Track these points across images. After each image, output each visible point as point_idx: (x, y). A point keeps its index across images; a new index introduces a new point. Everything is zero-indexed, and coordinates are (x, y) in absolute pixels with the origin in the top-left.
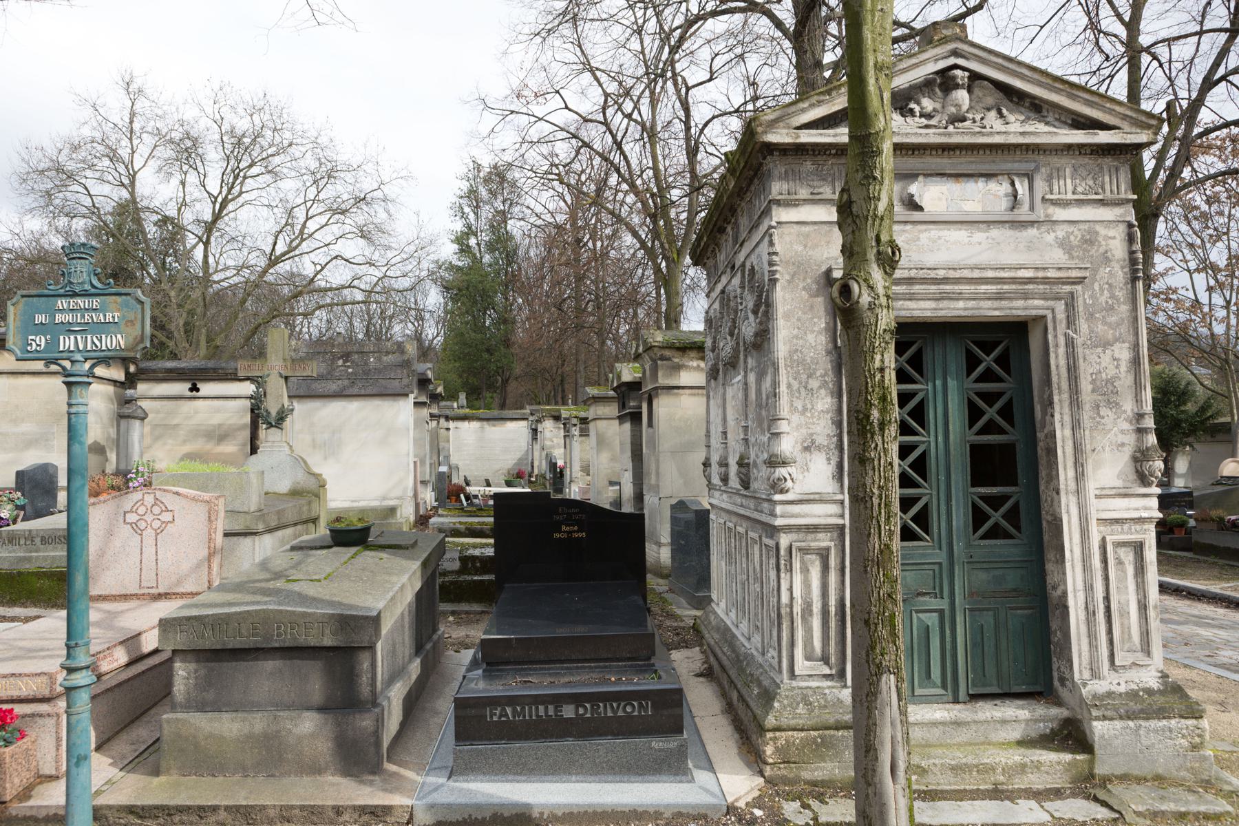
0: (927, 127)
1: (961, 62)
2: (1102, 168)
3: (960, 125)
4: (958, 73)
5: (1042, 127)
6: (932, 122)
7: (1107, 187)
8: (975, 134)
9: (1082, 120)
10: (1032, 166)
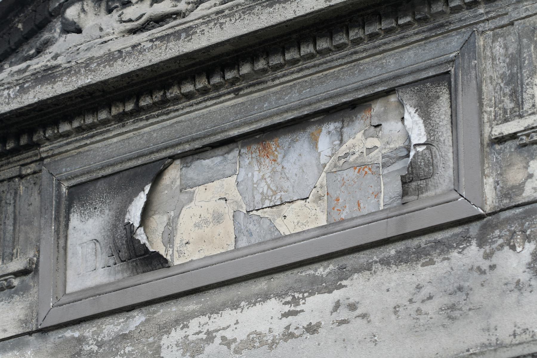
10: (452, 44)
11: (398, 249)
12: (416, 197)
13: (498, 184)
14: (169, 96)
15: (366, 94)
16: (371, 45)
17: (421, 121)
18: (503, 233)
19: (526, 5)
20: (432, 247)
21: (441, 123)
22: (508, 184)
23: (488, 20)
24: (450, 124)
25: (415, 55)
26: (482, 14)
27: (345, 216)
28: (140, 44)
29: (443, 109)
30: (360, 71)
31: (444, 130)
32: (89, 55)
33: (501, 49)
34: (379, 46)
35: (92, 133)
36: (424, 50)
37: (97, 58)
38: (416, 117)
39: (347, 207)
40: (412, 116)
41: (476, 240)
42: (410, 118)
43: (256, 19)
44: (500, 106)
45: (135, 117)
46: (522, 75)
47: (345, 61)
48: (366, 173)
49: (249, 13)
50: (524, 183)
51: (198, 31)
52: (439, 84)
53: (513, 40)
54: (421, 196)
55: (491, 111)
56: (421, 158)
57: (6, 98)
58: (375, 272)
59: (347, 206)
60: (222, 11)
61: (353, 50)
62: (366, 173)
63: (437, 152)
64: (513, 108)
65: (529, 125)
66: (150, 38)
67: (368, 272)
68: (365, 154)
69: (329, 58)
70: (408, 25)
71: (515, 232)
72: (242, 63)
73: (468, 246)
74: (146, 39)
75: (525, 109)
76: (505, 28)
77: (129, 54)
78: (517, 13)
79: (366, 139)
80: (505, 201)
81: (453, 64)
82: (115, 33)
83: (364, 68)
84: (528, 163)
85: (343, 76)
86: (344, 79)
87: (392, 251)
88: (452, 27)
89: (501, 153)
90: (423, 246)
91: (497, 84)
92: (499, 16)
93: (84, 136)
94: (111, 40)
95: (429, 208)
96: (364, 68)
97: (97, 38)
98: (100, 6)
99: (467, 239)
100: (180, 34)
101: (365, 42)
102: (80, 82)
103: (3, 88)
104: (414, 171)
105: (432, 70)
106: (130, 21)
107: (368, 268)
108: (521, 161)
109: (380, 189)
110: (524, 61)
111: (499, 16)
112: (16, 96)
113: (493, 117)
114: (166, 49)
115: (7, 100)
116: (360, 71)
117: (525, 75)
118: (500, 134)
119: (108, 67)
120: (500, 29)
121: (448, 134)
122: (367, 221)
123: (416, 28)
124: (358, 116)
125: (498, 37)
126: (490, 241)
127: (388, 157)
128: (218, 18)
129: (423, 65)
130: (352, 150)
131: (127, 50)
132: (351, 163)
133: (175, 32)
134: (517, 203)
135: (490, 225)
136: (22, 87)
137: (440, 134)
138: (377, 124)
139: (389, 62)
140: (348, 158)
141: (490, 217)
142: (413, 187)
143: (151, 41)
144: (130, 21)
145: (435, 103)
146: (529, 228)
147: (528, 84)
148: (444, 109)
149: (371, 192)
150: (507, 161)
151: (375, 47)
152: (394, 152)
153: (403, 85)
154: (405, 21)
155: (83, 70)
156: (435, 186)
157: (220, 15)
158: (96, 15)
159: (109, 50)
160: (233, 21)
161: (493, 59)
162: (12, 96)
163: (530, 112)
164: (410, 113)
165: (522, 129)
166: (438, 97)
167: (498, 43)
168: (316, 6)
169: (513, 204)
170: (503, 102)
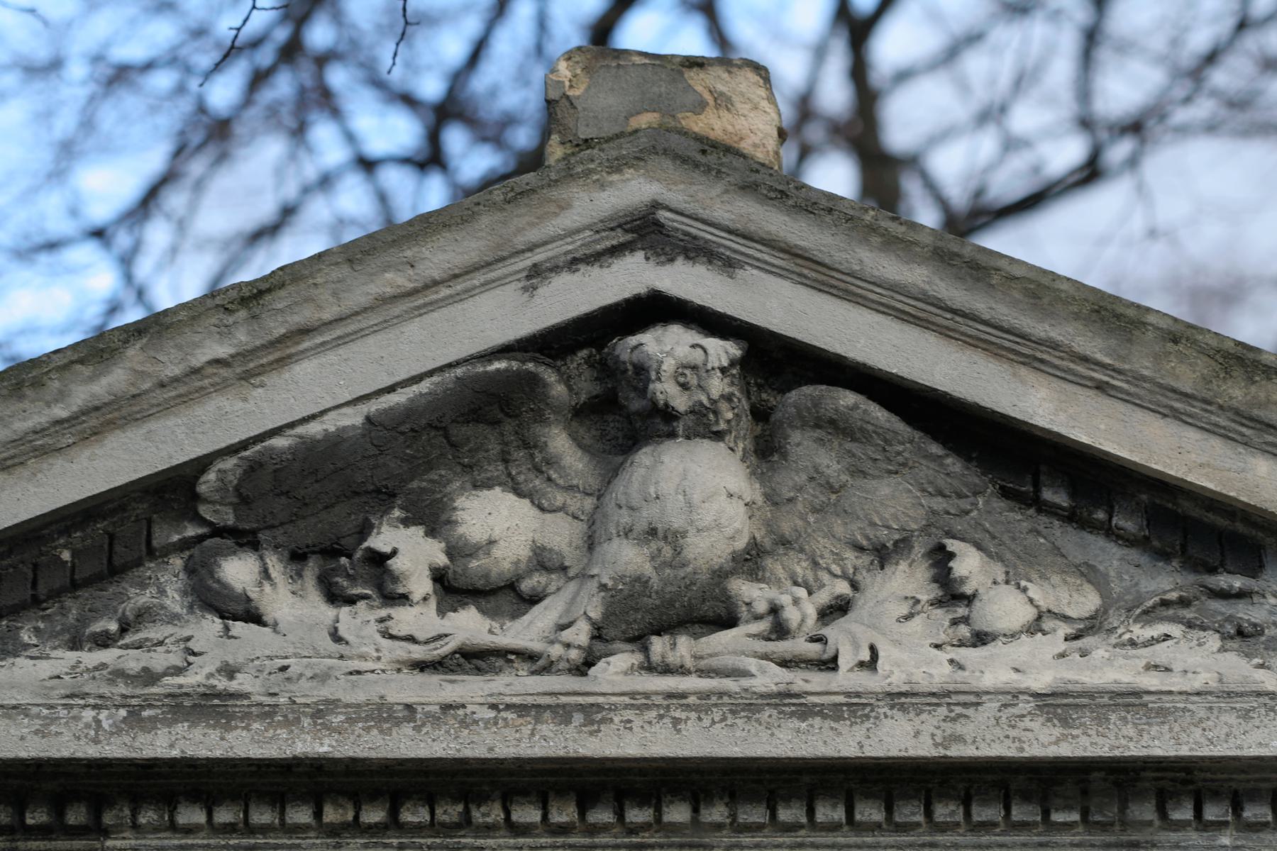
0: (474, 659)
1: (685, 281)
3: (684, 648)
4: (667, 346)
5: (1197, 660)
6: (526, 631)
8: (750, 706)
14: (477, 815)
28: (464, 706)
32: (325, 692)
35: (253, 841)
37: (347, 706)
43: (765, 735)
45: (372, 837)
49: (749, 718)
51: (616, 719)
57: (88, 726)
60: (683, 695)
61: (928, 839)
66: (490, 700)
69: (869, 840)
72: (669, 797)
74: (482, 700)
77: (435, 720)
82: (383, 660)
93: (231, 842)
94: (373, 671)
97: (330, 657)
98: (300, 575)
100: (570, 712)
101: (961, 831)
102: (300, 745)
103: (82, 702)
106: (411, 639)
112: (119, 732)
114: (533, 734)
115: (92, 733)
119: (375, 732)
121: (159, 750)
123: (1079, 834)
128: (668, 707)
131: (427, 708)
133: (558, 705)
136: (134, 714)
143: (494, 707)
144: (411, 639)
155: (306, 722)
157: (675, 701)
158: (293, 593)
159: (382, 697)
160: (706, 722)
162: (105, 725)
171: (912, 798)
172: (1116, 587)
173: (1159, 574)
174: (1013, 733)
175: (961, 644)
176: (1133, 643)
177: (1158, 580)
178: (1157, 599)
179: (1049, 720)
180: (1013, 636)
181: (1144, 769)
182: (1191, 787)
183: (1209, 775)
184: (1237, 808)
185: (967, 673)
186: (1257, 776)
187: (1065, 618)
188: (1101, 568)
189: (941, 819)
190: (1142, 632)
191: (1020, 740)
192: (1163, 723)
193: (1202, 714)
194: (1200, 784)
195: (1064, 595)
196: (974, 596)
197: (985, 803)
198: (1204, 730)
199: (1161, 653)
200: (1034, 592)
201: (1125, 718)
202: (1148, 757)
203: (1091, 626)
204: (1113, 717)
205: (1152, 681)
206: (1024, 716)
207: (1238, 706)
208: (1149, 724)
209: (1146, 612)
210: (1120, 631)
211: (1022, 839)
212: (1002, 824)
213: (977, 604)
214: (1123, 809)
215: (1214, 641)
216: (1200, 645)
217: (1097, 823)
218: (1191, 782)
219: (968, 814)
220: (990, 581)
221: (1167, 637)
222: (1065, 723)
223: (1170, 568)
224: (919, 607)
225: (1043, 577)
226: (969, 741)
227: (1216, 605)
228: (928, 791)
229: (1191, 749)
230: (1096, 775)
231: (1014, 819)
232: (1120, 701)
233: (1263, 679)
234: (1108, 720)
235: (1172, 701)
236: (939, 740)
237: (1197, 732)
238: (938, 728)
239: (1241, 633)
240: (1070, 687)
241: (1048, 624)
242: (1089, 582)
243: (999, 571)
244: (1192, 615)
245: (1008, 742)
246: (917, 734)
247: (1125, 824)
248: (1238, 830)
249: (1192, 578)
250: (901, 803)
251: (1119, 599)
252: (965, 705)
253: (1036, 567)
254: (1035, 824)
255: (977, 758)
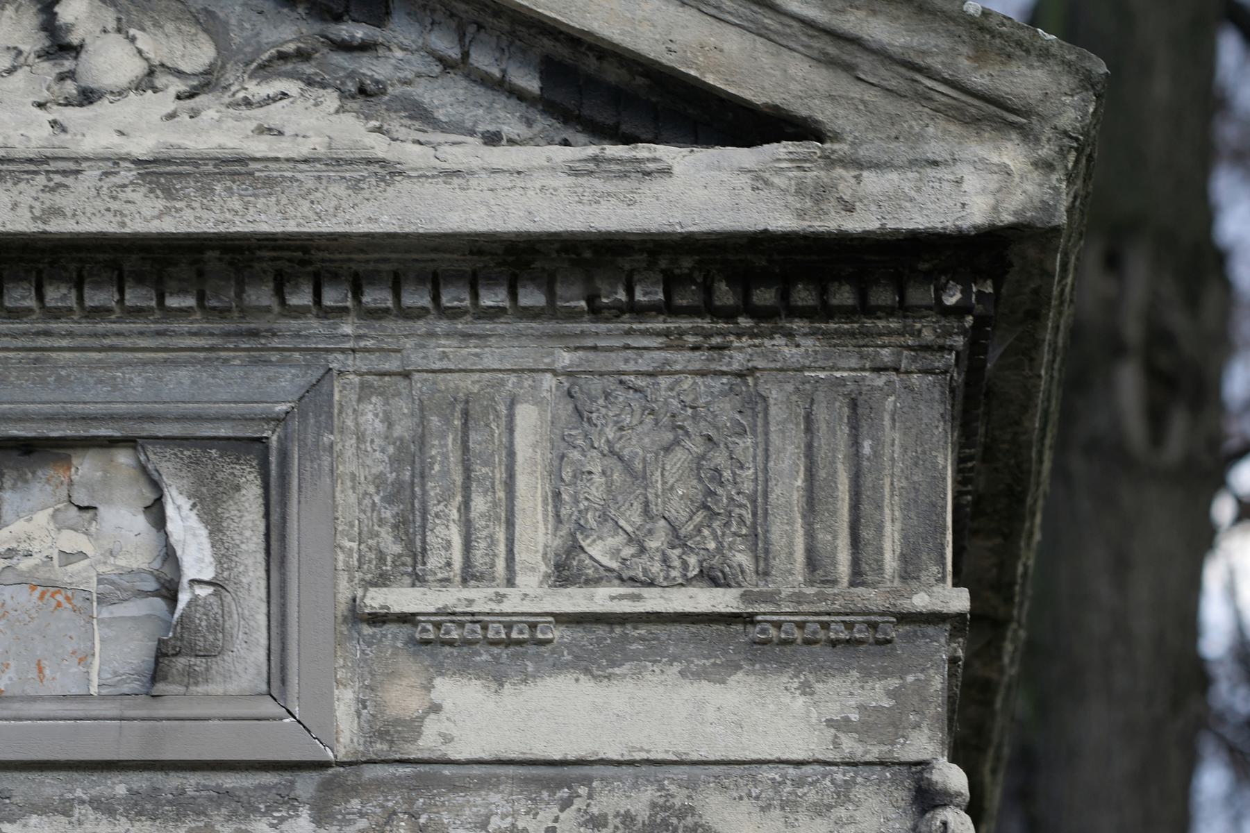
2: (755, 404)
5: (311, 121)
7: (788, 535)
9: (613, 74)
10: (281, 387)
11: (135, 787)
12: (182, 689)
13: (365, 707)
15: (69, 433)
16: (86, 326)
17: (203, 532)
18: (369, 808)
19: (444, 346)
20: (210, 799)
21: (243, 546)
22: (388, 712)
23: (354, 351)
24: (263, 552)
25: (193, 382)
26: (347, 336)
27: (6, 685)
29: (248, 517)
30: (59, 379)
31: (250, 562)
33: (377, 421)
34: (105, 335)
36: (214, 377)
38: (193, 520)
39: (12, 668)
40: (183, 514)
41: (310, 809)
42: (178, 518)
44: (370, 542)
46: (425, 492)
47: (19, 343)
48: (59, 605)
50: (421, 719)
52: (238, 459)
53: (406, 411)
54: (193, 689)
55: (351, 550)
56: (202, 610)
58: (80, 823)
59: (12, 663)
61: (42, 326)
62: (59, 605)
63: (234, 607)
64: (400, 556)
65: (446, 607)
67: (64, 820)
68: (56, 562)
70: (185, 312)
71: (395, 813)
73: (291, 817)
75: (429, 566)
76: (387, 378)
78: (423, 358)
79: (59, 530)
80: (379, 746)
81: (277, 426)
83: (69, 376)
84: (431, 680)
85: (18, 378)
86: (20, 386)
87: (119, 786)
88: (276, 343)
89: (373, 644)
90: (190, 792)
91: (366, 493)
92: (381, 350)
95: (217, 722)
96: (69, 376)
99: (292, 803)
101: (76, 318)
104: (185, 635)
105: (228, 425)
107: (65, 809)
108: (417, 672)
109: (93, 647)
110: (432, 464)
111: (381, 350)
113: (356, 563)
116: (59, 379)
117: (432, 493)
118: (382, 607)
120: (377, 378)
122: (75, 714)
123: (197, 321)
124: (39, 473)
125: (372, 393)
126: (340, 817)
127: (112, 583)
129: (213, 409)
130: (24, 546)
132: (21, 574)
134: (406, 757)
135: (340, 786)
137: (241, 569)
138: (86, 504)
139: (131, 379)
140: (15, 561)
141: (342, 769)
142: (180, 666)
145: (232, 498)
146: (424, 811)
147: (437, 515)
148: (250, 517)
149: (70, 649)
150: (386, 665)
151: (95, 335)
152: (127, 577)
153: (157, 438)
154: (183, 305)
156: (224, 676)
161: (360, 438)
163: (440, 576)
164: (179, 508)
165: (433, 610)
166: (238, 488)
167: (371, 407)
168: (12, 222)
169: (397, 757)
170: (377, 535)
171: (22, 280)
172: (236, 38)
173: (283, 22)
174: (115, 205)
175: (68, 103)
176: (248, 103)
177: (280, 29)
178: (273, 51)
179: (152, 191)
180: (121, 93)
181: (260, 248)
182: (310, 269)
183: (327, 255)
184: (357, 293)
185: (68, 137)
186: (377, 256)
187: (179, 73)
188: (221, 15)
189: (52, 304)
190: (258, 90)
191: (121, 214)
192: (270, 194)
193: (310, 184)
194: (319, 265)
195: (177, 44)
196: (81, 46)
197: (98, 285)
198: (312, 202)
199: (275, 114)
200: (144, 41)
201: (230, 188)
202: (255, 233)
203: (205, 83)
204: (218, 188)
205: (260, 147)
206: (125, 186)
207: (347, 175)
208: (254, 195)
209: (262, 67)
210: (233, 89)
211: (139, 326)
212: (117, 310)
213: (83, 55)
214: (239, 294)
215: (331, 100)
216: (316, 105)
217: (214, 308)
218: (310, 263)
219: (80, 299)
220: (98, 29)
221: (284, 95)
222: (169, 193)
223: (295, 15)
224: (22, 59)
225: (157, 24)
226: (69, 214)
227: (339, 59)
228: (39, 272)
229: (299, 225)
230: (210, 254)
231: (127, 303)
232: (225, 169)
233: (374, 144)
234: (213, 190)
235: (280, 170)
236: (37, 213)
237: (306, 205)
238: (36, 199)
239: (362, 91)
240: (173, 153)
241: (160, 80)
242: (206, 31)
243: (109, 17)
244: (312, 71)
245: (109, 216)
246: (15, 206)
247: (244, 312)
248: (360, 317)
249: (318, 27)
250: (11, 285)
251: (240, 51)
252: (64, 173)
253: (151, 13)
254: (150, 310)
255: (79, 234)
